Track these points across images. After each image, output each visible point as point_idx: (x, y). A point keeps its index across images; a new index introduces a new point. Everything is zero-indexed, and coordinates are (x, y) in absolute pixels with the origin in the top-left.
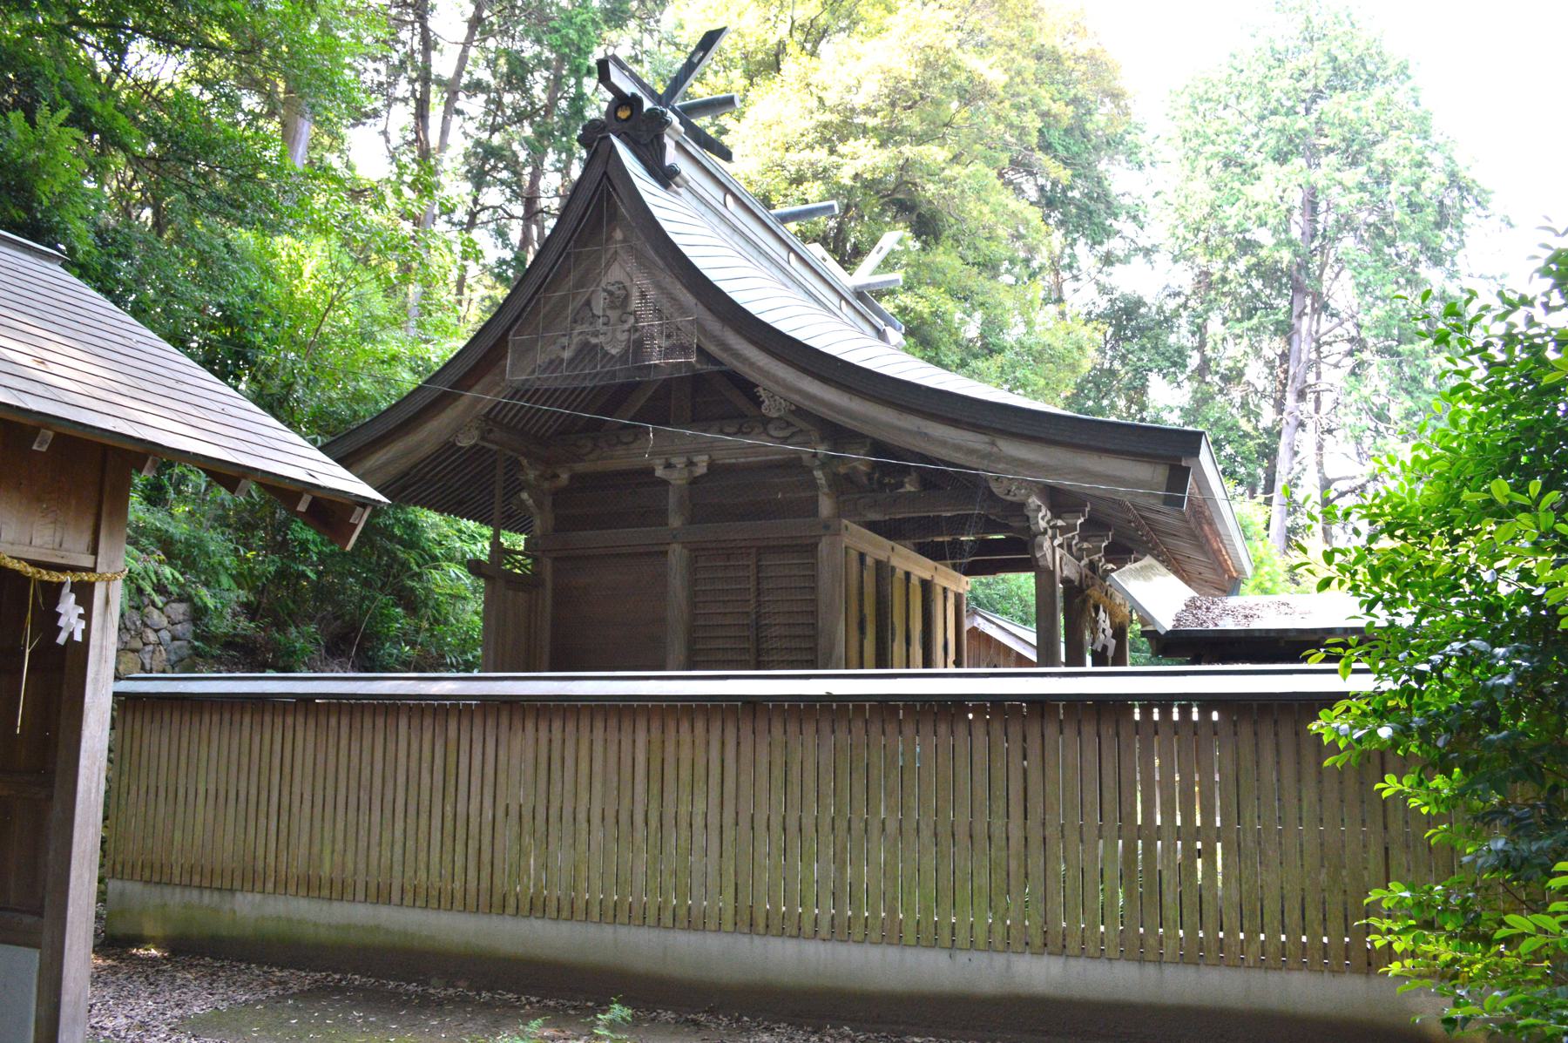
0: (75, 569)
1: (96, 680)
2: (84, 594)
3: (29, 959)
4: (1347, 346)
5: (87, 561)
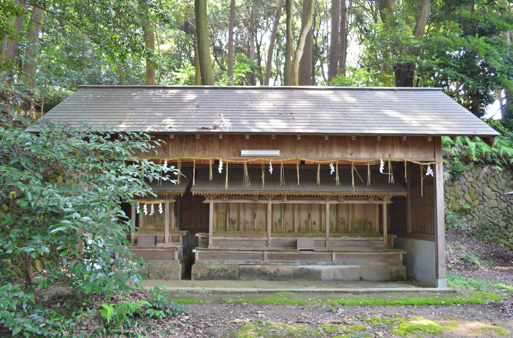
0: (430, 162)
1: (439, 185)
2: (433, 167)
3: (433, 243)
4: (123, 265)
5: (433, 159)
